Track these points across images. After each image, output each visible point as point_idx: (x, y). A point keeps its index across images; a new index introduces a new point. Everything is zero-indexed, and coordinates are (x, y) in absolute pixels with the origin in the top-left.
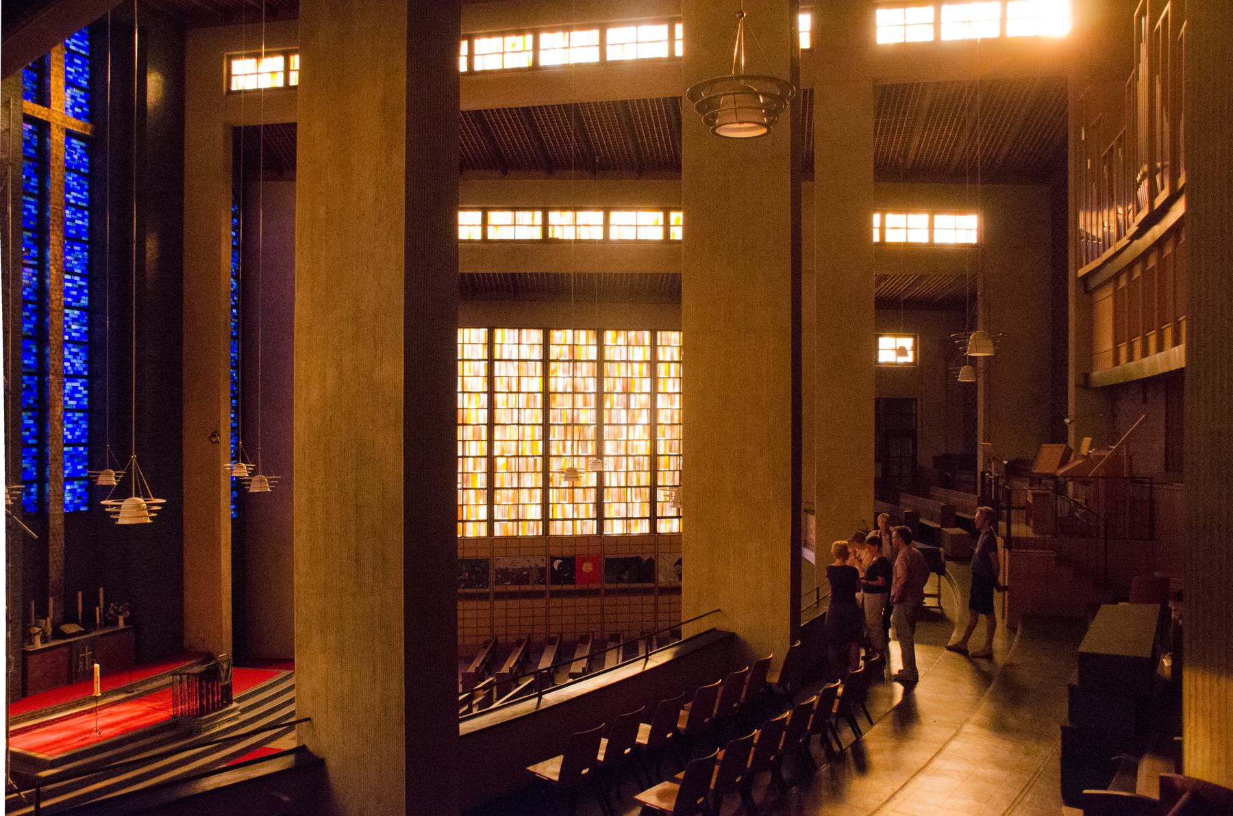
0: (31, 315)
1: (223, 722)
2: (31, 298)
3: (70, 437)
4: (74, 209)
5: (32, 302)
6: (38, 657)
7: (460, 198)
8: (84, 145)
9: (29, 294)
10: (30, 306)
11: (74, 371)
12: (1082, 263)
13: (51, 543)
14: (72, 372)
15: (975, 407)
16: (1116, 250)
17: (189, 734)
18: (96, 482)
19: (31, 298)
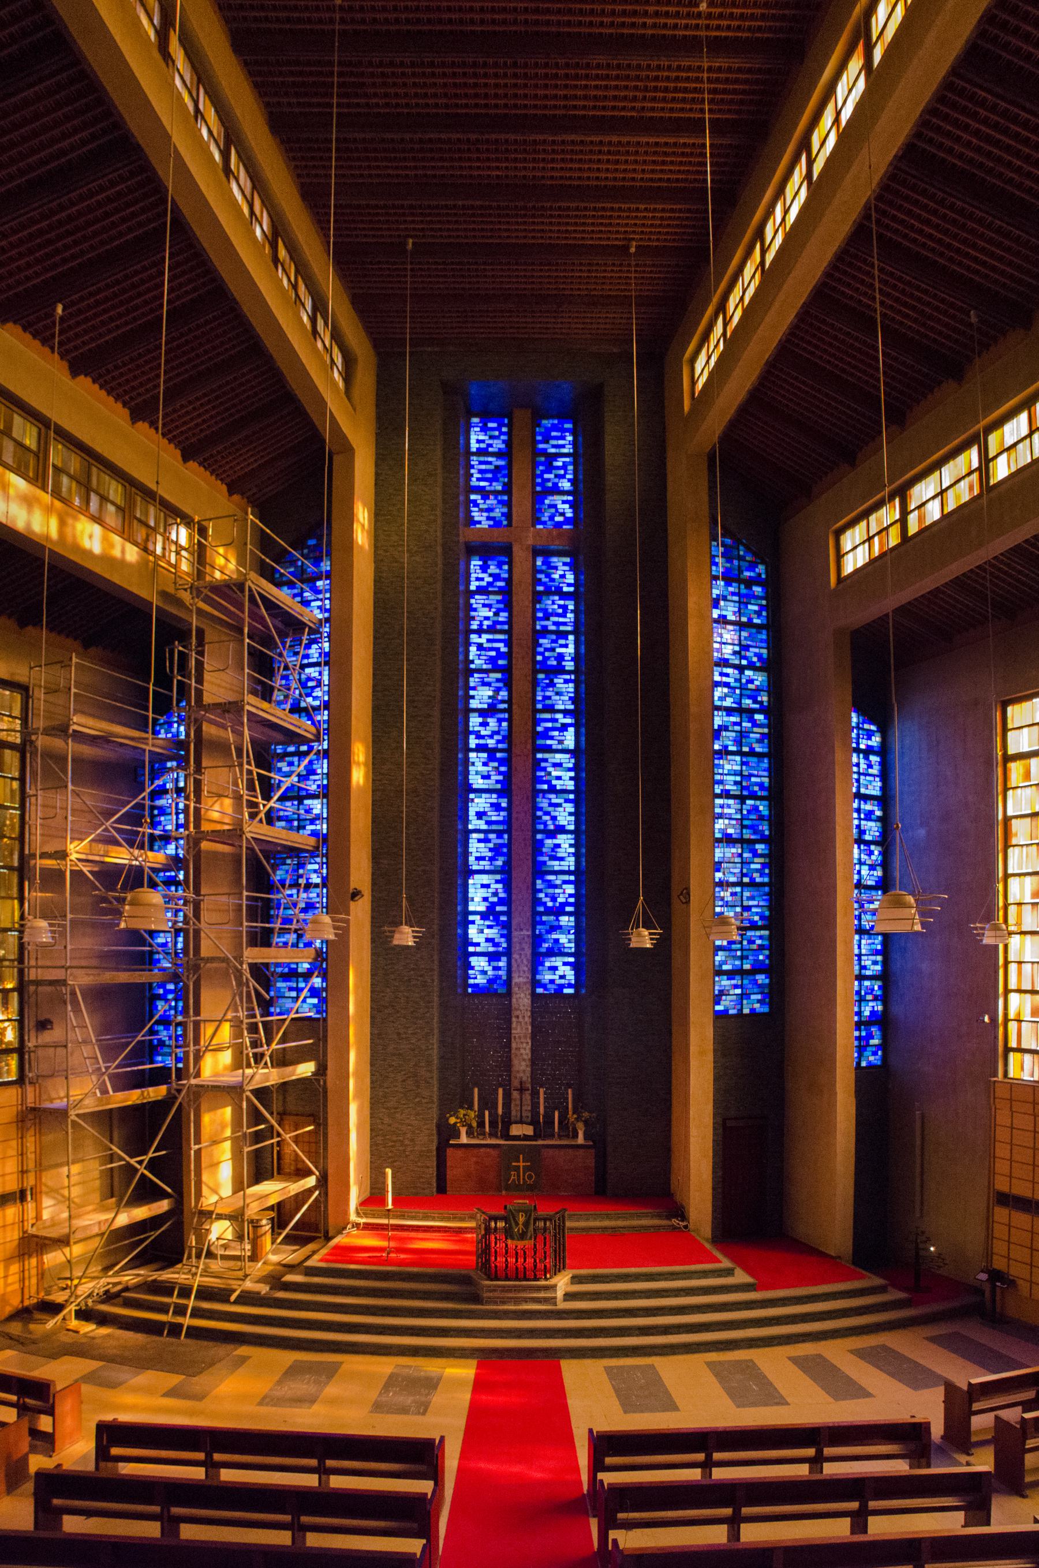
0: (500, 765)
1: (526, 1300)
2: (500, 746)
3: (550, 904)
4: (554, 637)
5: (501, 751)
6: (460, 1153)
7: (53, 635)
8: (568, 560)
9: (498, 742)
10: (499, 755)
11: (555, 826)
12: (238, 616)
13: (514, 1025)
14: (552, 827)
15: (504, 1104)
16: (937, 473)
17: (476, 1299)
18: (981, 940)
19: (500, 746)
